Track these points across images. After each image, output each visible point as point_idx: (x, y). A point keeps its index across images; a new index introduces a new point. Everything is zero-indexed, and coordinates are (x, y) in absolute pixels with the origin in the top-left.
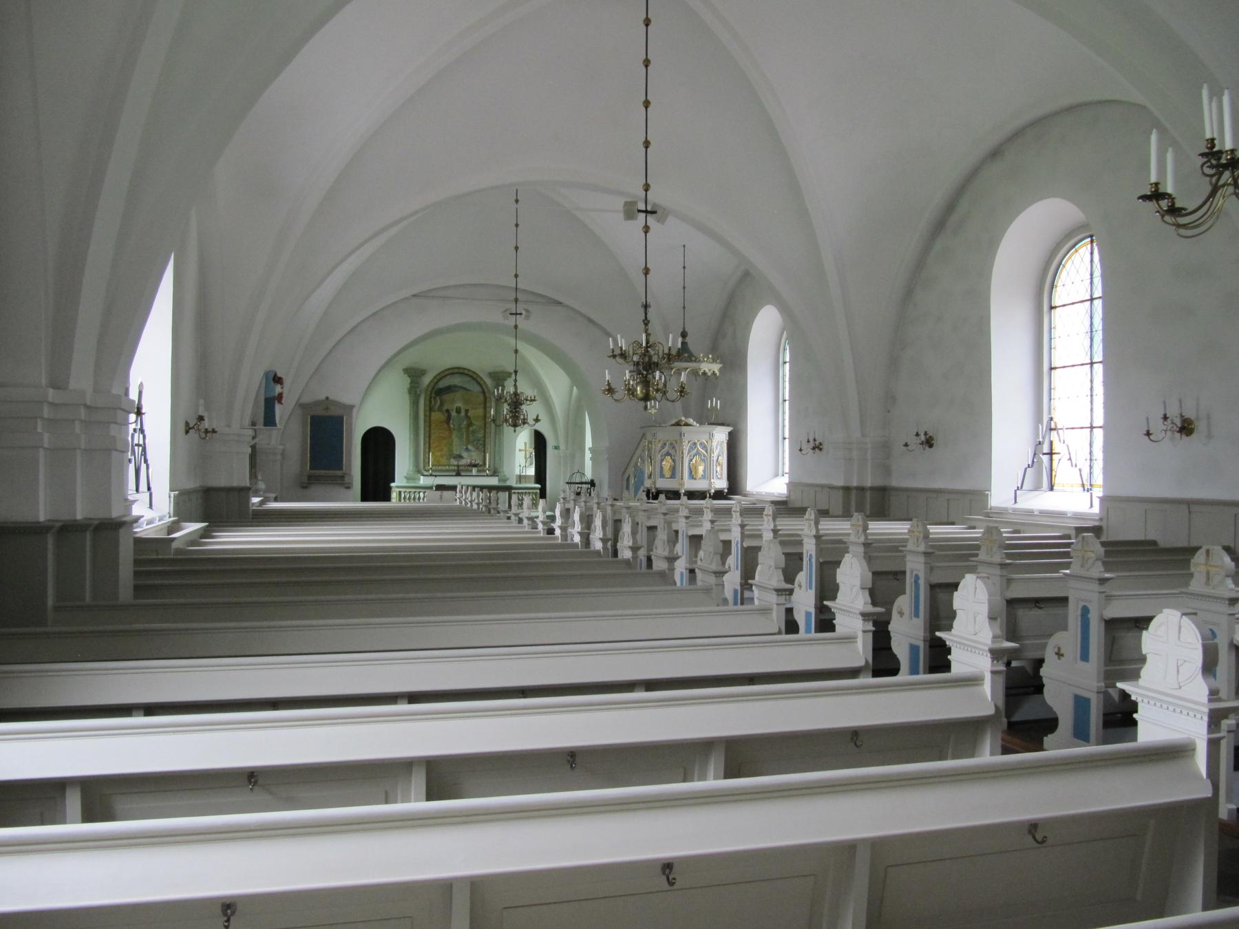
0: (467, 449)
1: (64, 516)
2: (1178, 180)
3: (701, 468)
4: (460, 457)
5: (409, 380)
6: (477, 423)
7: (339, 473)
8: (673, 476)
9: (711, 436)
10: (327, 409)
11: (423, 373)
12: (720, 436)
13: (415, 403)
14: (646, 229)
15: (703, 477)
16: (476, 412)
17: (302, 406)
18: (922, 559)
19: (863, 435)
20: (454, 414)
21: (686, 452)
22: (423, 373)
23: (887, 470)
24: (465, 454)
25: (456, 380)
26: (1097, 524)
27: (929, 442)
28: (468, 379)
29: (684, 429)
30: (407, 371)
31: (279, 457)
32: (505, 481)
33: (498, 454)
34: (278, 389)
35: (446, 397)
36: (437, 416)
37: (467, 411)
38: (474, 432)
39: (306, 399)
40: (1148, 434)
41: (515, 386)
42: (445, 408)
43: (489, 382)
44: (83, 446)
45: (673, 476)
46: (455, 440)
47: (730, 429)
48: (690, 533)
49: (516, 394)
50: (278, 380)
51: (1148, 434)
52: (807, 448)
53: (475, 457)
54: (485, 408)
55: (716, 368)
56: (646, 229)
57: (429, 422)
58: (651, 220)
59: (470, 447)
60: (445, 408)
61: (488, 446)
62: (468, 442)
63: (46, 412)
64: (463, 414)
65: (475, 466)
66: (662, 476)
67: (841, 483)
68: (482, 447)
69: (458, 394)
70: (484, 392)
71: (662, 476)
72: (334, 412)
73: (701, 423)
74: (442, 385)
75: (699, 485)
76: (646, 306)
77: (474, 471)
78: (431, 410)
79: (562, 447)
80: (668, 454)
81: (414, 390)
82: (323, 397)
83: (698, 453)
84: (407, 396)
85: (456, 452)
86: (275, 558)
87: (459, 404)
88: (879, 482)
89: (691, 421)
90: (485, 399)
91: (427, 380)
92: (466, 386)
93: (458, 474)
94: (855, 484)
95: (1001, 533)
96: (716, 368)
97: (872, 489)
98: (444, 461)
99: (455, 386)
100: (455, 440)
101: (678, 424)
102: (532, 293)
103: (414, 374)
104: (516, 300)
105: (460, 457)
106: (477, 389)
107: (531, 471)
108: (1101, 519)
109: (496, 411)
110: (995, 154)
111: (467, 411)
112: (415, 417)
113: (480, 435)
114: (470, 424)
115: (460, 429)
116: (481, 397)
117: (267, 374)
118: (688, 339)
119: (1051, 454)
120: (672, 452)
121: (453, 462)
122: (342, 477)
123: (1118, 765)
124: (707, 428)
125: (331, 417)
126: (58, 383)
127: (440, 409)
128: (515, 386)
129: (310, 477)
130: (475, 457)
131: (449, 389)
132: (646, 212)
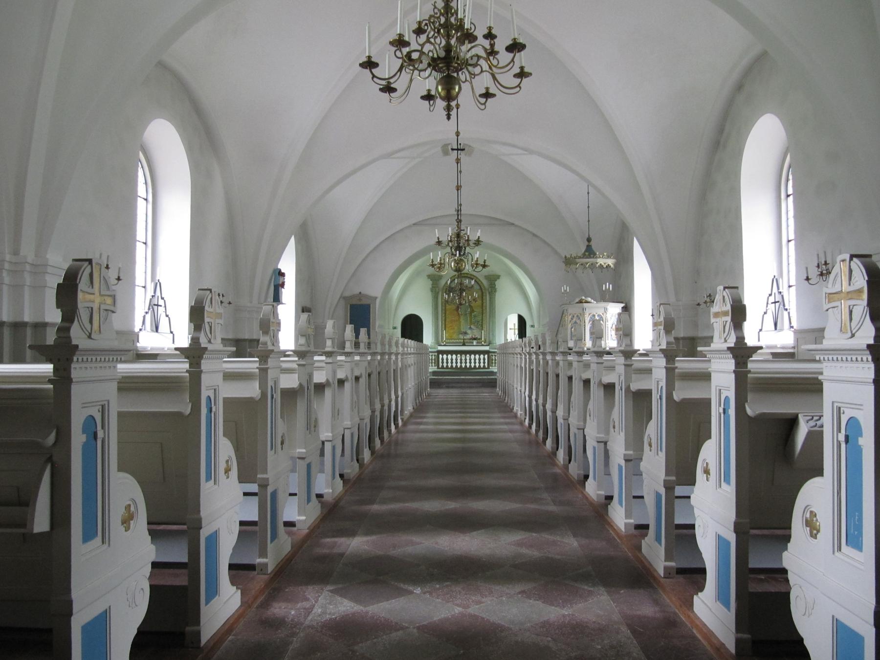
1: (18, 320)
4: (466, 333)
6: (477, 310)
9: (606, 310)
10: (360, 300)
12: (614, 310)
13: (435, 298)
14: (458, 161)
17: (343, 298)
18: (623, 367)
19: (677, 300)
23: (696, 325)
24: (469, 331)
26: (792, 351)
33: (492, 331)
38: (475, 316)
39: (347, 294)
40: (808, 279)
43: (485, 283)
44: (28, 284)
47: (623, 305)
48: (634, 387)
51: (808, 279)
53: (476, 333)
55: (611, 262)
56: (458, 161)
57: (445, 311)
58: (462, 155)
61: (484, 326)
62: (471, 323)
63: (28, 267)
65: (475, 339)
72: (364, 302)
77: (475, 343)
81: (435, 290)
82: (357, 292)
84: (430, 293)
85: (463, 330)
86: (242, 373)
88: (690, 334)
89: (589, 299)
93: (464, 345)
94: (682, 336)
96: (611, 262)
97: (684, 338)
98: (455, 336)
101: (581, 302)
105: (466, 333)
108: (794, 348)
110: (739, 87)
113: (479, 318)
114: (472, 311)
118: (592, 243)
121: (461, 337)
124: (603, 304)
126: (16, 252)
130: (476, 333)
132: (458, 150)
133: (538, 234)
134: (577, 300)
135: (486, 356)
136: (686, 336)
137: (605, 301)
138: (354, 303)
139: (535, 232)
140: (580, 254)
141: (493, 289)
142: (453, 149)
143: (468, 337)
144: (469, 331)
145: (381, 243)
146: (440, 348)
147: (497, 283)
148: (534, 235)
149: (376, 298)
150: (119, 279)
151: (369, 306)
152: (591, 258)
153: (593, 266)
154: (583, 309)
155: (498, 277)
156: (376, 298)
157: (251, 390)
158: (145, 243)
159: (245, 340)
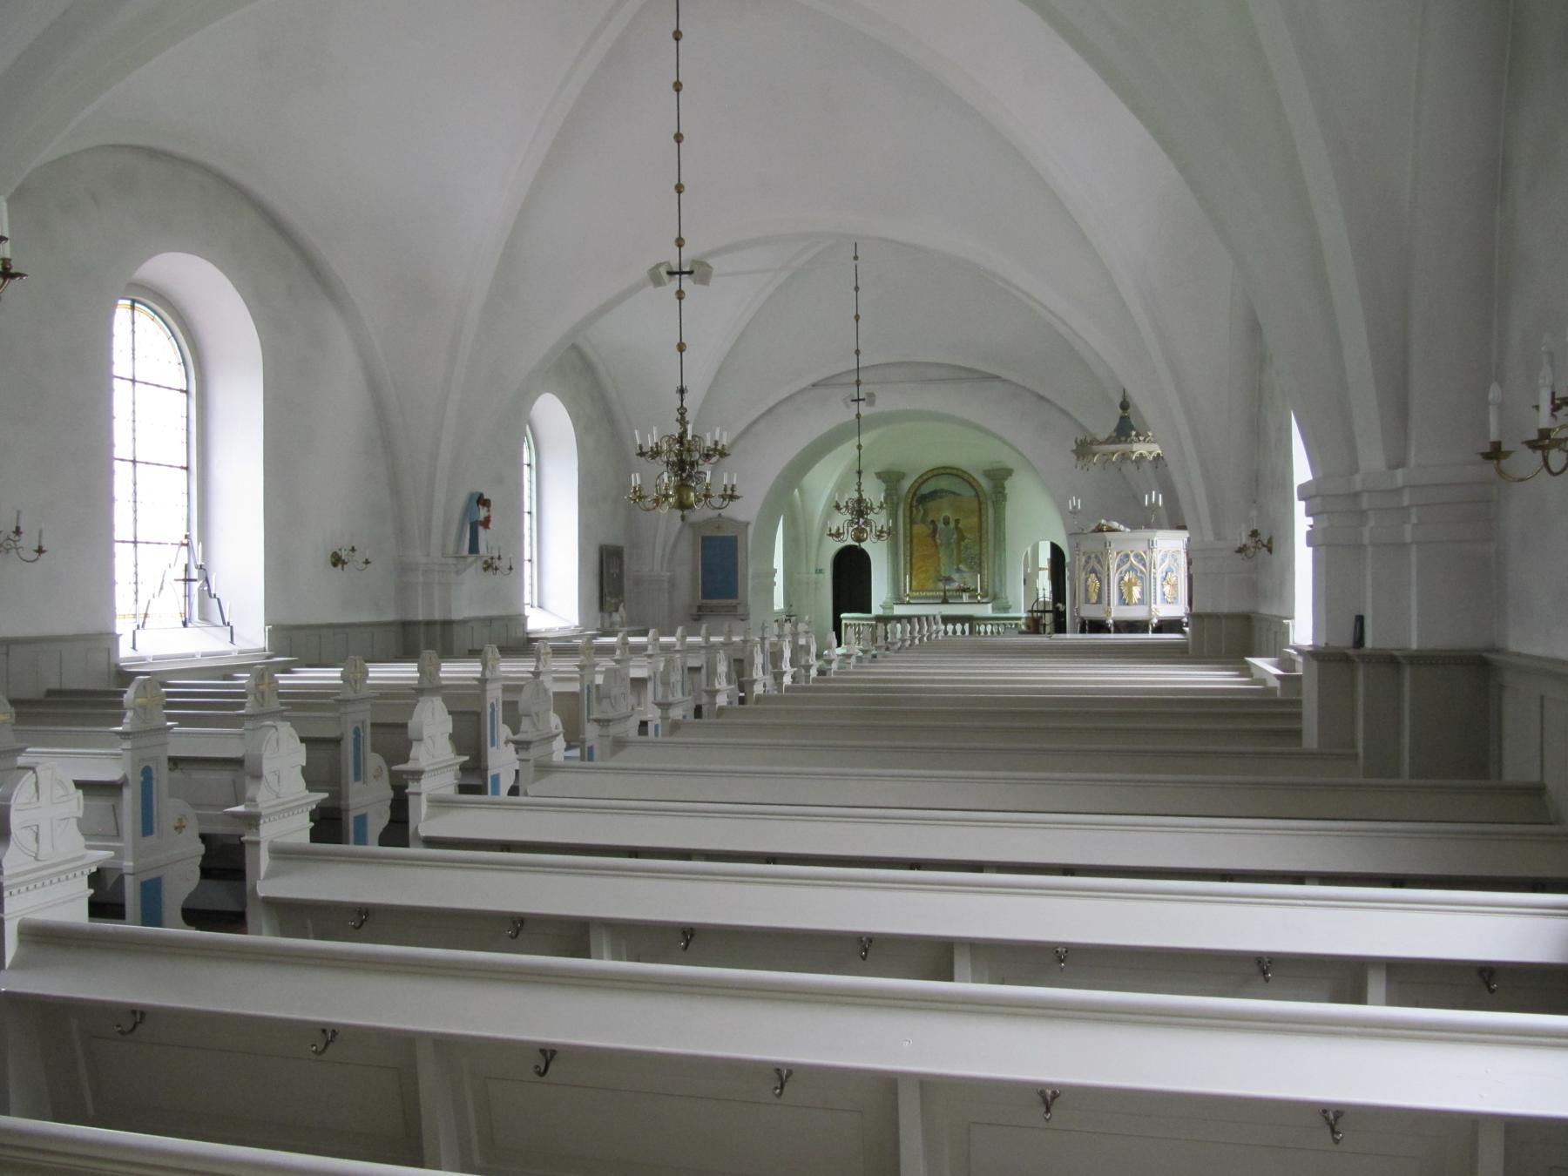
0: (958, 570)
2: (11, 231)
3: (1136, 591)
4: (949, 580)
5: (884, 486)
6: (971, 536)
7: (733, 602)
8: (1099, 601)
9: (1151, 545)
11: (901, 476)
14: (680, 295)
15: (1141, 602)
20: (941, 525)
21: (1113, 568)
22: (901, 476)
24: (956, 576)
25: (943, 483)
27: (337, 560)
28: (957, 480)
29: (1108, 535)
31: (666, 585)
32: (1006, 609)
34: (483, 513)
35: (931, 505)
36: (920, 529)
37: (957, 521)
38: (966, 547)
41: (859, 490)
42: (929, 519)
43: (985, 483)
45: (1099, 601)
46: (944, 559)
49: (860, 501)
50: (482, 501)
51: (40, 551)
52: (503, 564)
56: (680, 295)
57: (910, 539)
60: (929, 519)
62: (960, 561)
64: (952, 525)
65: (964, 590)
66: (1087, 601)
67: (390, 616)
68: (977, 565)
70: (977, 495)
71: (1087, 601)
72: (728, 532)
73: (1134, 526)
74: (925, 490)
75: (1134, 613)
76: (682, 391)
78: (912, 522)
80: (1093, 571)
83: (1132, 568)
89: (1115, 525)
90: (980, 503)
91: (906, 485)
92: (953, 489)
93: (945, 601)
95: (276, 681)
97: (1230, 617)
98: (930, 585)
99: (942, 491)
100: (944, 559)
101: (1100, 529)
102: (961, 368)
104: (858, 383)
105: (949, 580)
106: (967, 492)
111: (957, 521)
113: (975, 551)
114: (961, 538)
115: (949, 544)
116: (975, 504)
117: (472, 496)
119: (187, 580)
120: (1098, 567)
121: (941, 585)
122: (740, 610)
124: (1144, 534)
125: (725, 538)
127: (923, 521)
128: (859, 490)
129: (700, 608)
131: (934, 495)
132: (681, 273)
133: (1046, 394)
134: (1093, 526)
135: (967, 626)
136: (1233, 610)
137: (1149, 526)
138: (708, 534)
139: (1041, 392)
140: (1101, 436)
141: (999, 495)
142: (671, 273)
143: (955, 585)
144: (956, 576)
145: (754, 423)
146: (899, 610)
147: (1007, 484)
148: (1041, 398)
149: (747, 524)
150: (40, 551)
151: (734, 539)
152: (1120, 442)
153: (1125, 457)
154: (1106, 544)
155: (1008, 473)
156: (747, 524)
157: (575, 687)
158: (187, 468)
159: (419, 623)
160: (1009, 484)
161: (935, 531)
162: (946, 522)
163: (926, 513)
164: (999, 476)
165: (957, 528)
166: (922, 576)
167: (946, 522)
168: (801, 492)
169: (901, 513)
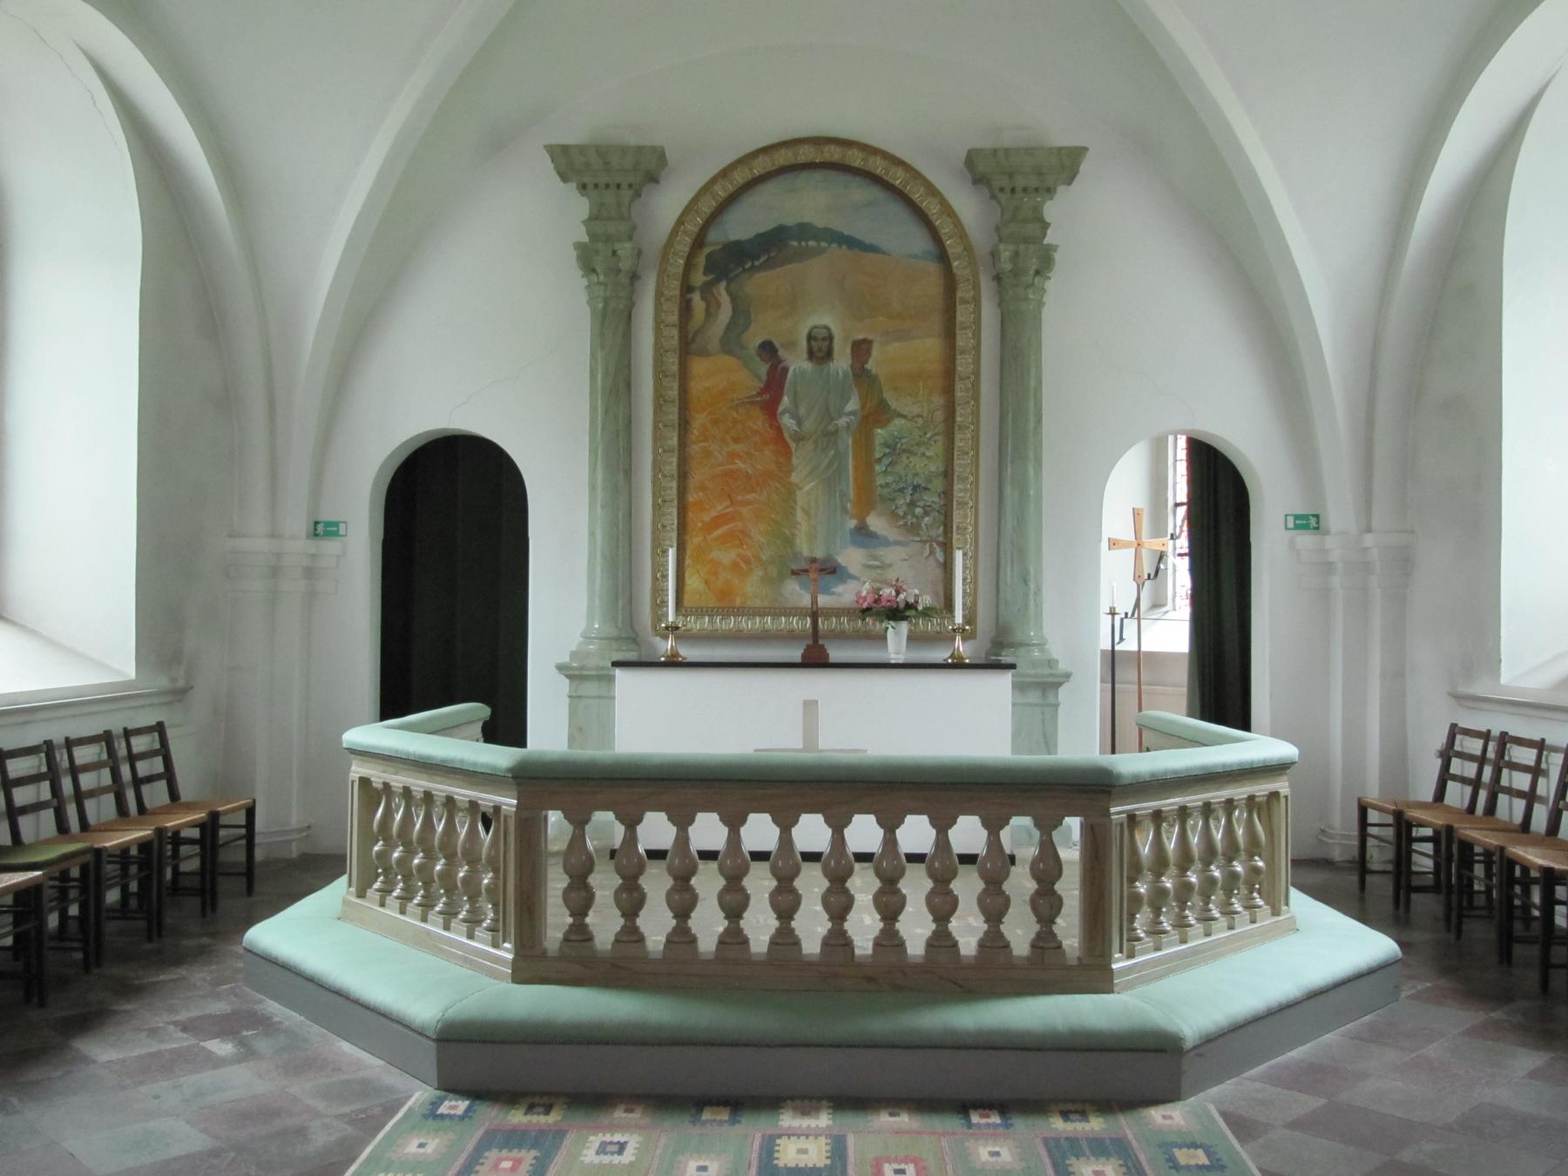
0: (863, 534)
4: (830, 570)
5: (581, 207)
6: (913, 408)
11: (647, 168)
13: (614, 323)
16: (905, 354)
20: (797, 363)
24: (851, 558)
25: (807, 202)
28: (861, 192)
30: (572, 163)
33: (1012, 558)
35: (762, 283)
36: (723, 376)
37: (861, 349)
43: (969, 208)
54: (950, 332)
57: (682, 411)
59: (876, 523)
60: (754, 338)
62: (867, 500)
64: (842, 362)
65: (896, 613)
69: (817, 270)
70: (943, 257)
74: (742, 225)
78: (688, 346)
79: (1340, 514)
81: (607, 260)
85: (805, 548)
87: (825, 318)
91: (668, 205)
98: (751, 588)
99: (804, 231)
103: (610, 177)
105: (830, 570)
106: (900, 237)
107: (1171, 633)
109: (83, 907)
111: (861, 349)
112: (616, 386)
113: (926, 464)
114: (877, 413)
115: (831, 436)
116: (930, 283)
121: (797, 593)
123: (1021, 553)
127: (731, 342)
130: (903, 569)
131: (773, 246)
141: (1023, 261)
143: (844, 595)
147: (1052, 210)
160: (1069, 216)
161: (775, 383)
162: (820, 349)
163: (742, 316)
164: (1022, 181)
165: (860, 373)
166: (726, 556)
167: (820, 349)
168: (995, 1126)
169: (620, 604)
